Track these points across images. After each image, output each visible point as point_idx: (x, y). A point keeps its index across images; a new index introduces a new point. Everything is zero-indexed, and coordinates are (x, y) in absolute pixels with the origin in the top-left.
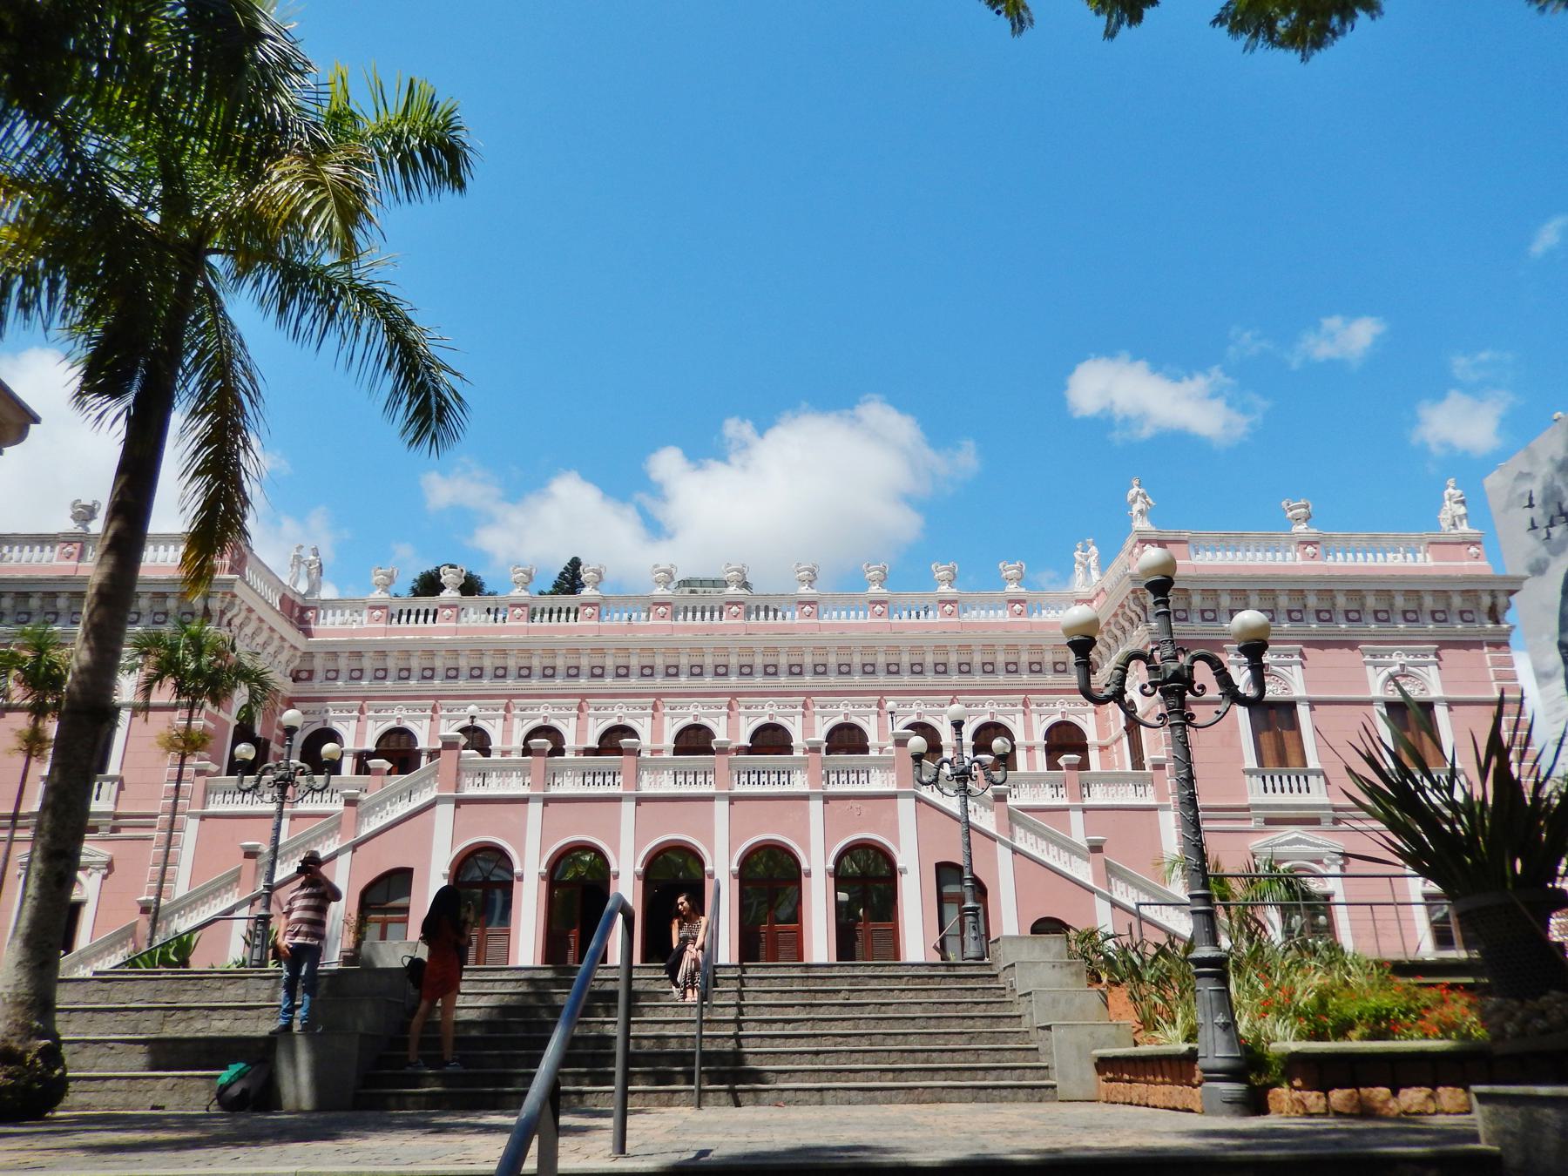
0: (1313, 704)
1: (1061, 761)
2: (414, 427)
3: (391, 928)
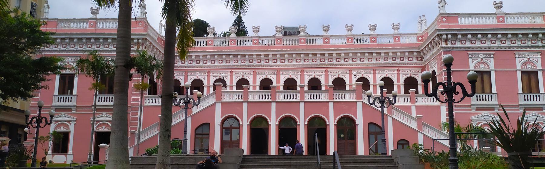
0: (495, 71)
1: (409, 91)
2: (234, 10)
3: (204, 140)
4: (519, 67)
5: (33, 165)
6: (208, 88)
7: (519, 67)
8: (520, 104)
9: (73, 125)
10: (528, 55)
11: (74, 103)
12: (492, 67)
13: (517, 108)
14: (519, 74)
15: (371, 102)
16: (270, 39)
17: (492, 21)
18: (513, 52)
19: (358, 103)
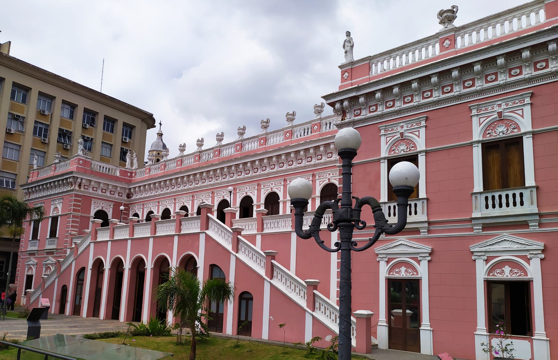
4: (477, 136)
5: (244, 326)
6: (285, 203)
7: (477, 136)
8: (474, 215)
10: (500, 105)
12: (525, 124)
13: (468, 225)
15: (306, 227)
17: (433, 52)
18: (463, 107)
19: (201, 235)
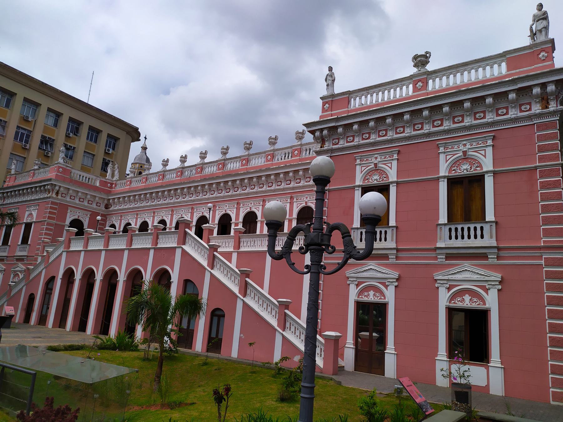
4: (443, 171)
7: (443, 171)
8: (438, 245)
9: (392, 289)
10: (465, 145)
11: (489, 241)
12: (488, 164)
13: (433, 254)
14: (443, 187)
16: (287, 151)
18: (432, 145)
